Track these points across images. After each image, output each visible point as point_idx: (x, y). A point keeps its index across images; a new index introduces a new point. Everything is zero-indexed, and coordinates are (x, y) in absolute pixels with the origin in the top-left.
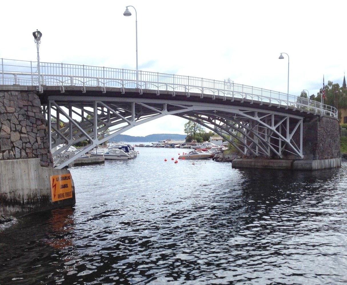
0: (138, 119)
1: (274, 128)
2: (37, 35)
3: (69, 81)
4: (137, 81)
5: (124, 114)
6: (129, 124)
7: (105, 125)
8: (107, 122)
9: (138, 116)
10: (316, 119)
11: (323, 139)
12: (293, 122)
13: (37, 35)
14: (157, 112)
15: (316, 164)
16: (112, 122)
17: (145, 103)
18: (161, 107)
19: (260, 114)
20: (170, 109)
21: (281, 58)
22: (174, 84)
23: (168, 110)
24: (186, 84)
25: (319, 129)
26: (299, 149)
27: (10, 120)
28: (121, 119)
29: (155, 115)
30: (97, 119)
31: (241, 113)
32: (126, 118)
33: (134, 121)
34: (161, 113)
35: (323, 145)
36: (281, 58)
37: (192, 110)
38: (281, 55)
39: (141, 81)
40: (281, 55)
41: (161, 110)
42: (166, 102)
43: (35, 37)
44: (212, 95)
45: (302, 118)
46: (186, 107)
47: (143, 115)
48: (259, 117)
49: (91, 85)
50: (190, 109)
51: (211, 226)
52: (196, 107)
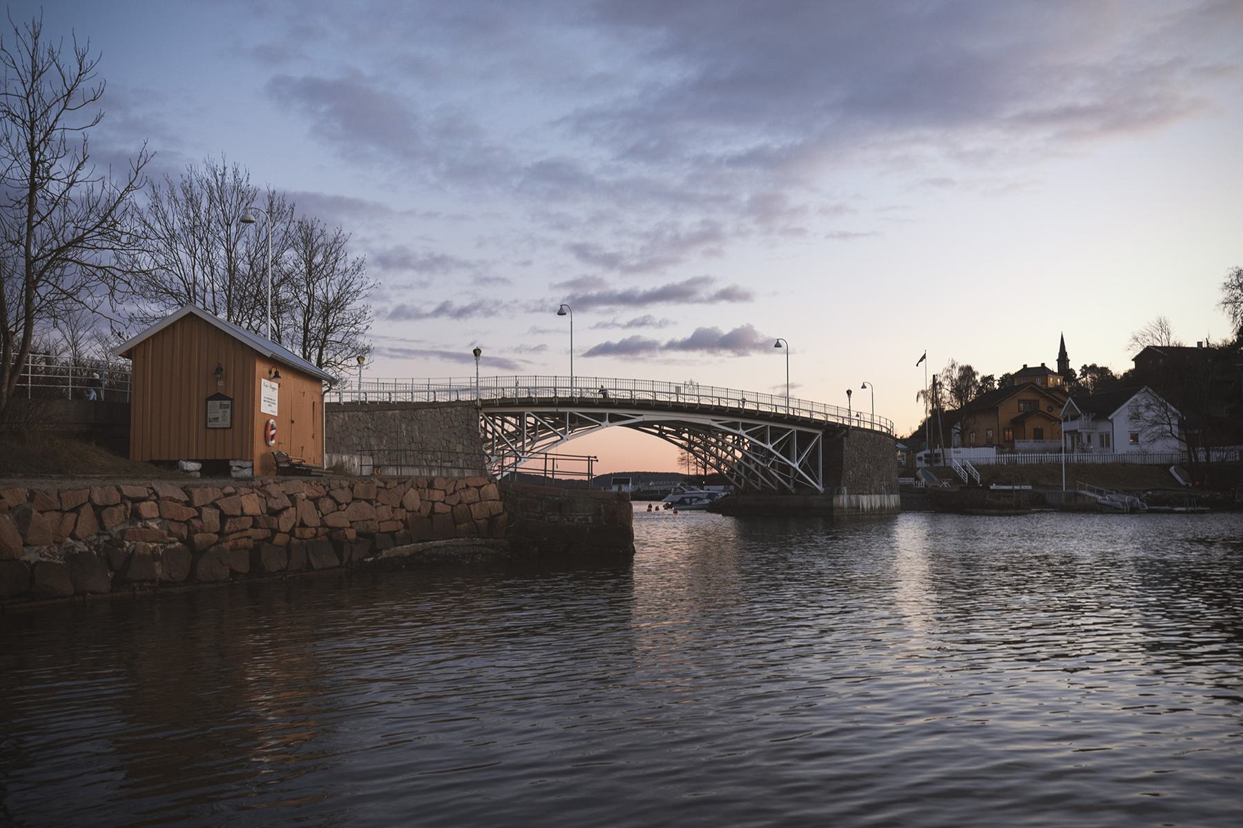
0: (572, 432)
1: (769, 446)
2: (849, 392)
3: (629, 395)
4: (571, 388)
5: (555, 426)
6: (562, 438)
7: (532, 439)
8: (535, 435)
9: (572, 429)
10: (843, 433)
11: (854, 464)
12: (804, 439)
13: (849, 392)
14: (597, 424)
15: (843, 500)
16: (540, 436)
17: (579, 413)
18: (601, 418)
19: (745, 426)
20: (614, 419)
21: (864, 387)
22: (712, 397)
23: (611, 421)
24: (811, 409)
25: (846, 448)
26: (818, 476)
27: (455, 434)
28: (552, 432)
29: (591, 428)
30: (756, 439)
31: (715, 424)
32: (558, 430)
33: (567, 434)
34: (600, 425)
35: (853, 472)
36: (864, 387)
37: (642, 420)
38: (864, 385)
39: (576, 388)
40: (864, 385)
41: (601, 421)
42: (607, 411)
43: (848, 394)
44: (667, 402)
45: (820, 433)
46: (635, 417)
47: (579, 427)
48: (744, 429)
49: (872, 423)
50: (639, 419)
51: (963, 564)
52: (648, 416)
